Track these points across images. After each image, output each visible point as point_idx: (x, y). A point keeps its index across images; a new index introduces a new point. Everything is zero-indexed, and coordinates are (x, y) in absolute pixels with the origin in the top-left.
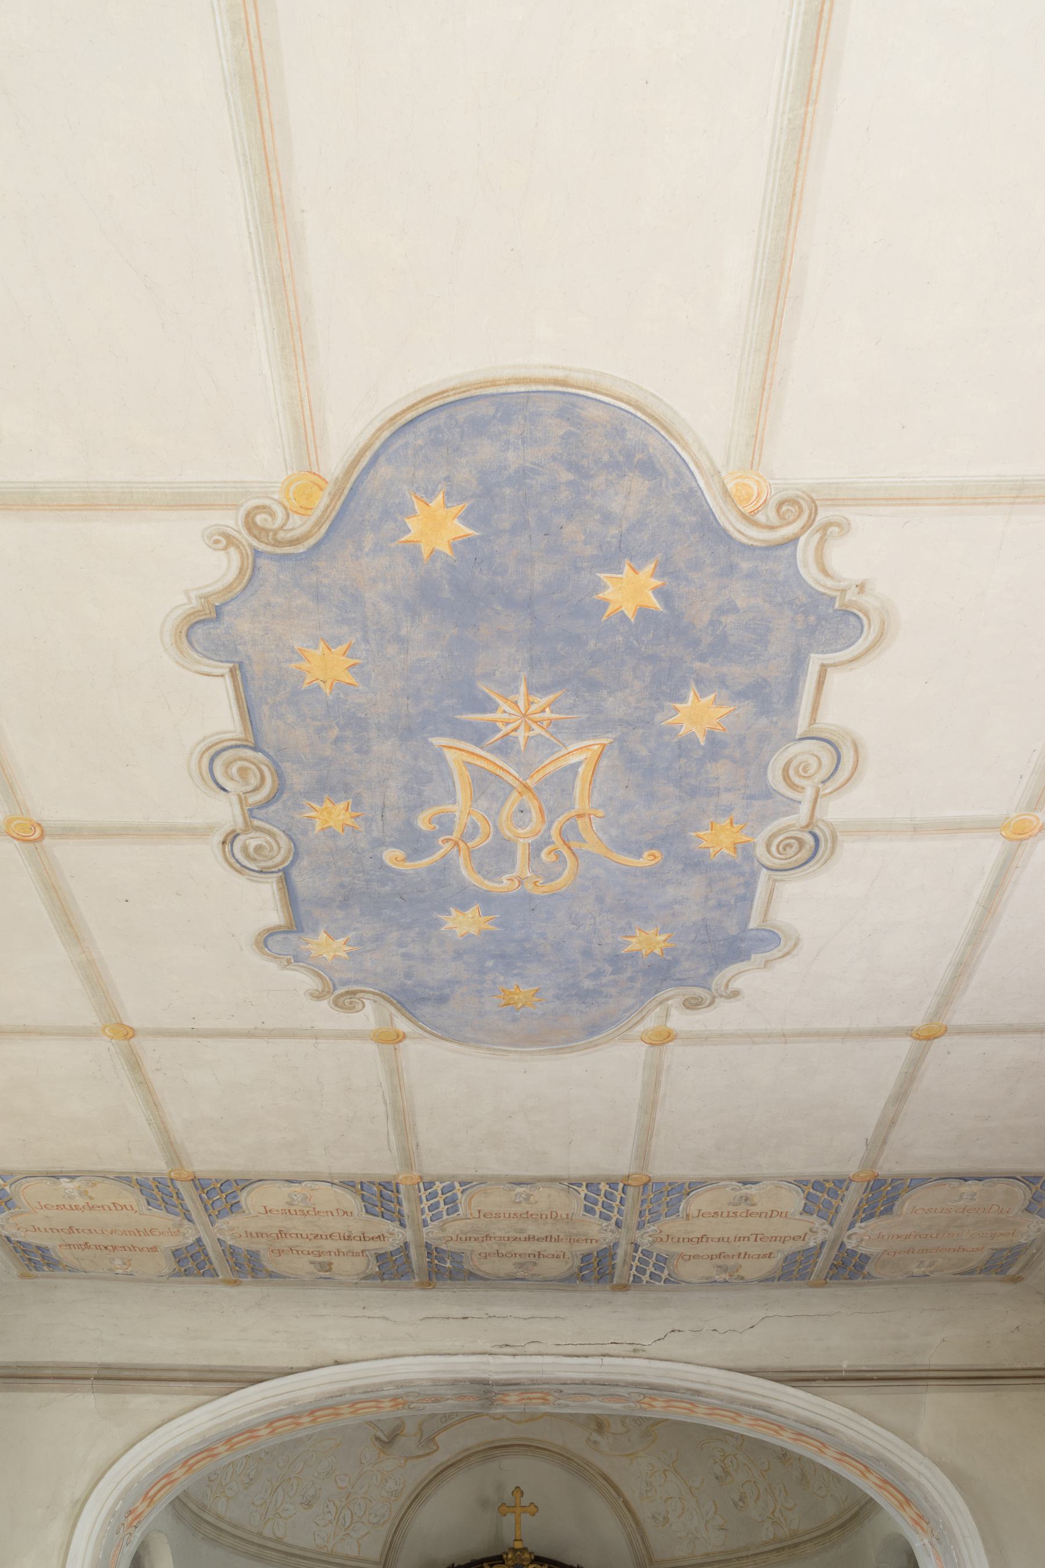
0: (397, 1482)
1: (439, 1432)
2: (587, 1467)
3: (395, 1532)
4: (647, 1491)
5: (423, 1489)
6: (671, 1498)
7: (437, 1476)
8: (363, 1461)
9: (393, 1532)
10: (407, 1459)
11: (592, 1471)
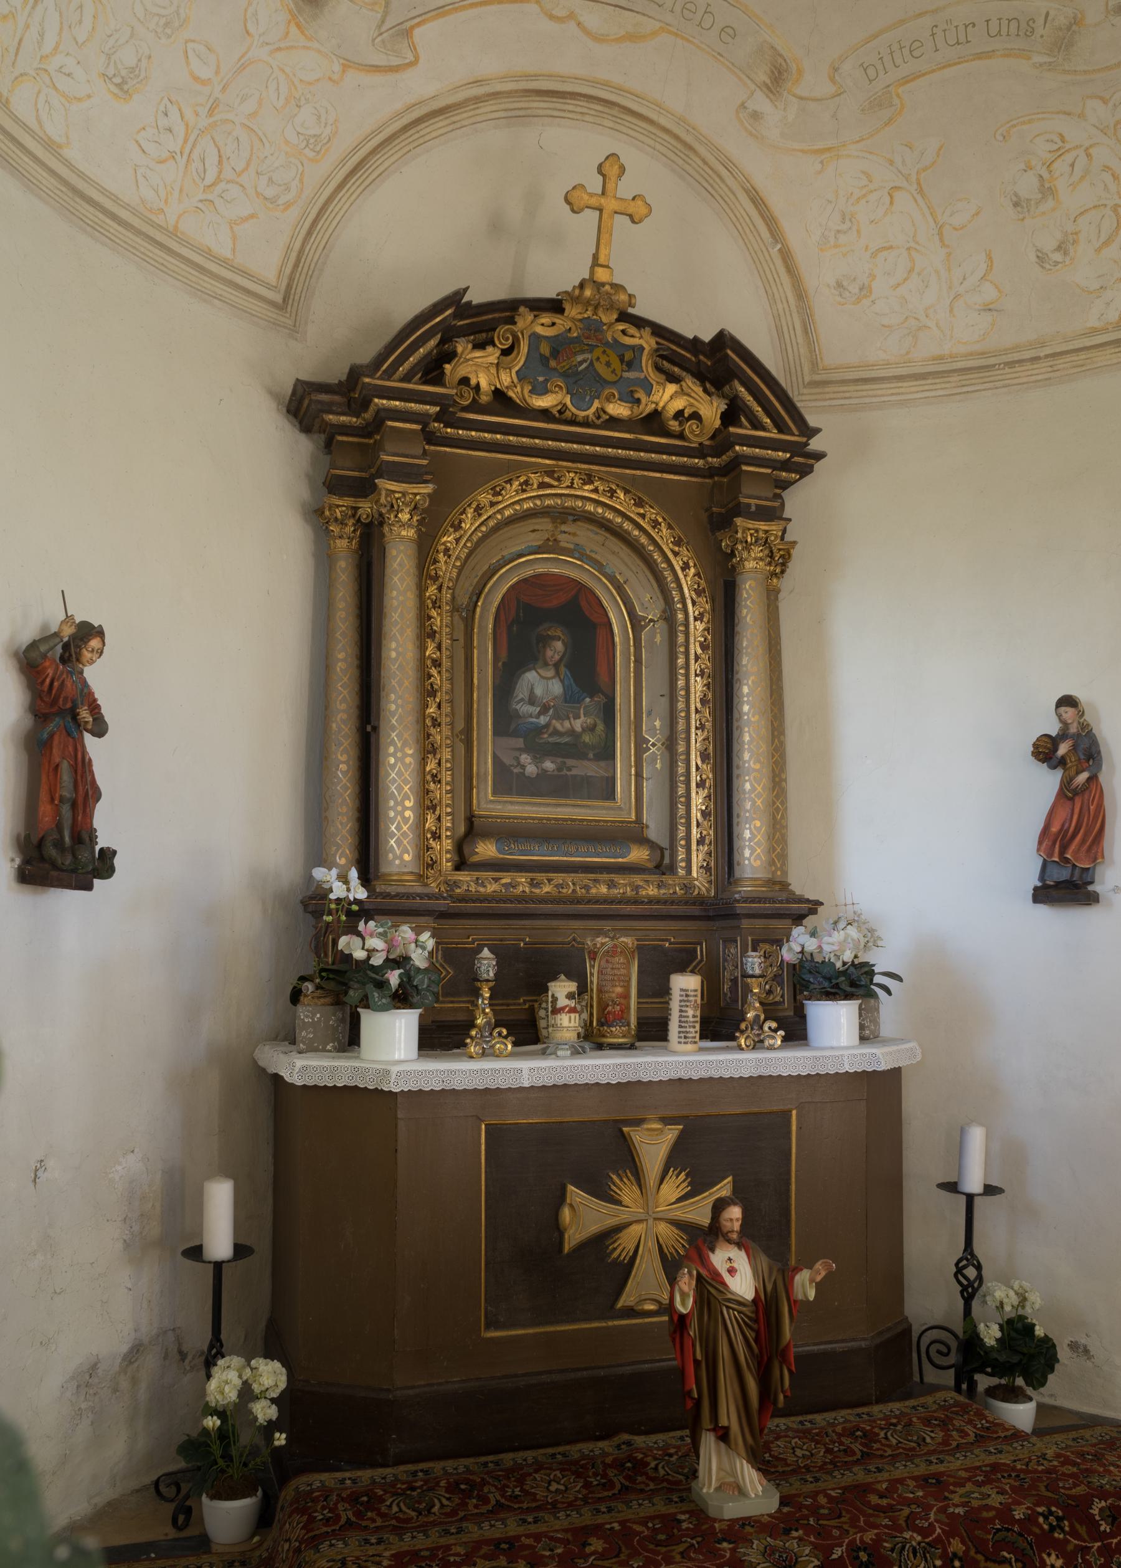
0: (319, 117)
1: (424, 17)
2: (724, 172)
3: (309, 233)
4: (838, 231)
5: (373, 152)
6: (891, 247)
7: (405, 129)
8: (251, 28)
9: (304, 232)
10: (348, 65)
11: (730, 180)
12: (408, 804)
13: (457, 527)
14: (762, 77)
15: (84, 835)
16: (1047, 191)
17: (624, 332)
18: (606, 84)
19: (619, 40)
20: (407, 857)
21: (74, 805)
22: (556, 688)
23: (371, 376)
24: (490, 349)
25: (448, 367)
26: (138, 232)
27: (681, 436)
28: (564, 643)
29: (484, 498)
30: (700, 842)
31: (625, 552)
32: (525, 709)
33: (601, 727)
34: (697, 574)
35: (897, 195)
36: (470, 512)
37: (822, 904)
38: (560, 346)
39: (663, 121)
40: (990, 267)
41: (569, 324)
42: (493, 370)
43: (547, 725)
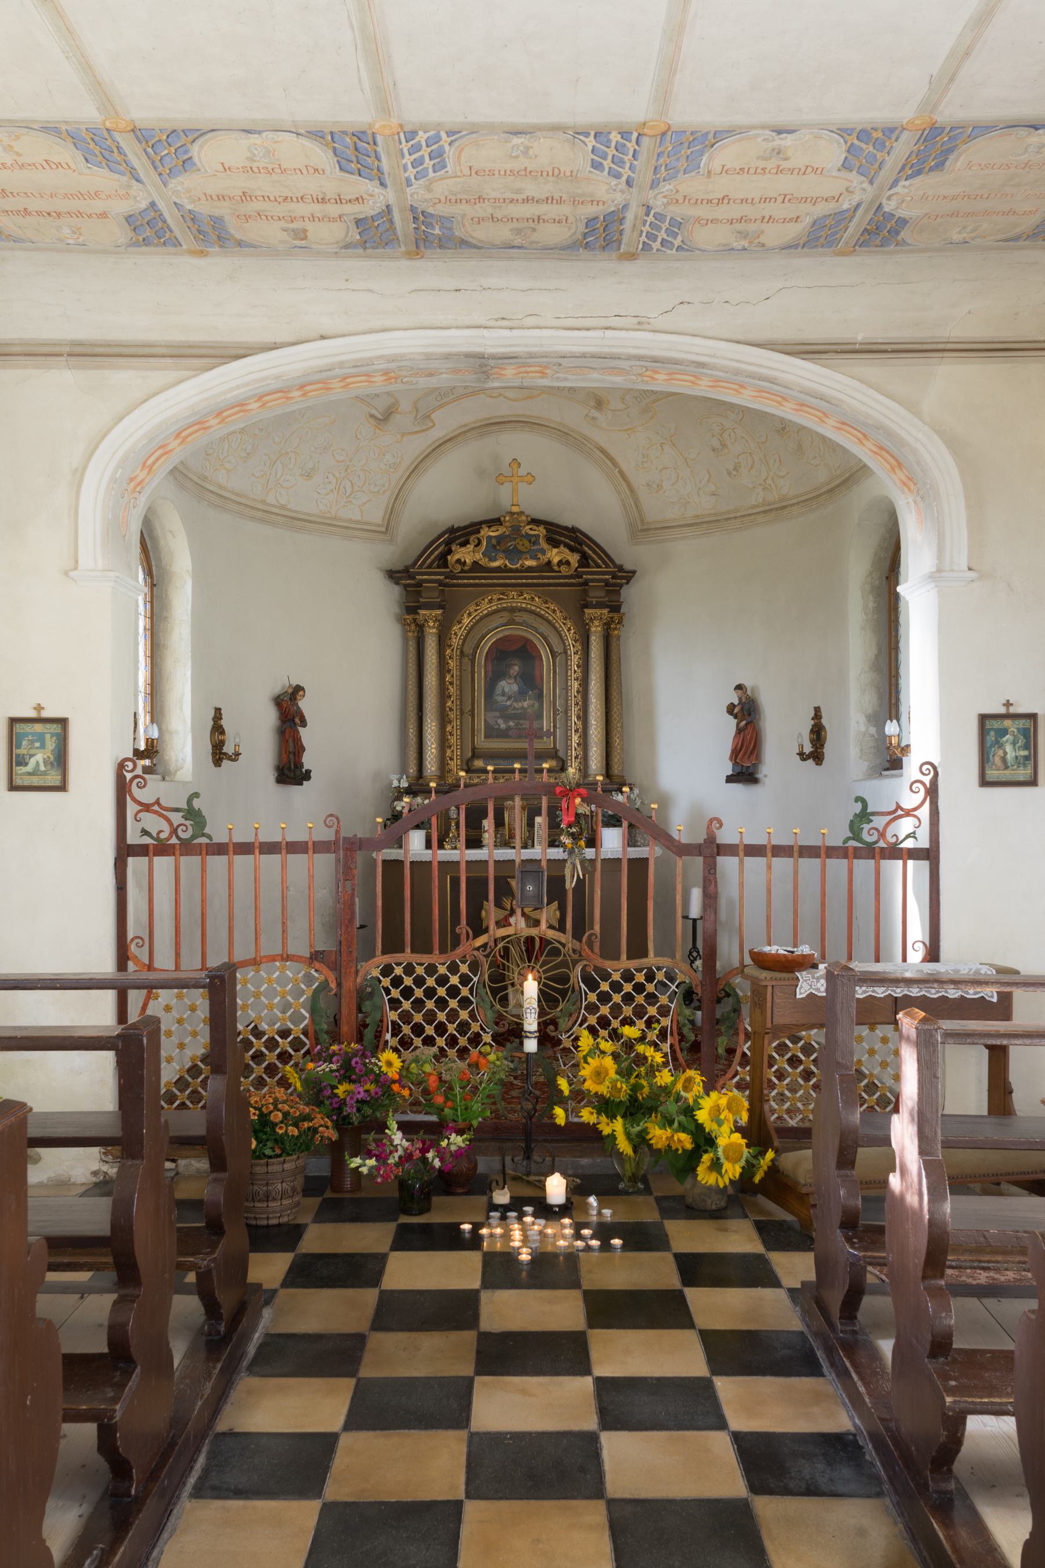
1: (434, 410)
2: (585, 442)
3: (396, 499)
5: (421, 462)
7: (434, 450)
11: (589, 445)
12: (433, 746)
13: (460, 622)
14: (593, 404)
15: (299, 765)
16: (724, 445)
17: (531, 529)
18: (523, 416)
19: (525, 399)
20: (433, 769)
21: (294, 754)
22: (515, 688)
23: (413, 568)
24: (468, 546)
25: (449, 557)
26: (320, 523)
27: (560, 572)
28: (519, 667)
29: (472, 608)
30: (576, 758)
31: (545, 623)
32: (500, 698)
33: (537, 705)
34: (575, 633)
35: (664, 446)
36: (465, 615)
37: (730, 779)
38: (500, 539)
39: (552, 425)
40: (710, 476)
41: (505, 529)
42: (472, 554)
43: (511, 705)
